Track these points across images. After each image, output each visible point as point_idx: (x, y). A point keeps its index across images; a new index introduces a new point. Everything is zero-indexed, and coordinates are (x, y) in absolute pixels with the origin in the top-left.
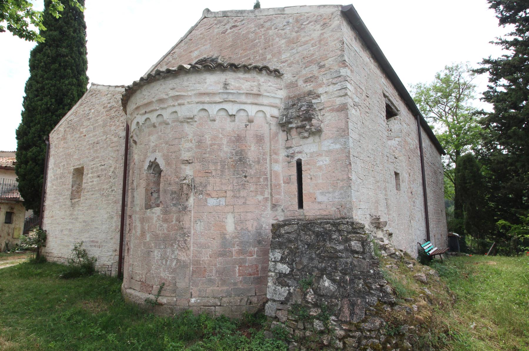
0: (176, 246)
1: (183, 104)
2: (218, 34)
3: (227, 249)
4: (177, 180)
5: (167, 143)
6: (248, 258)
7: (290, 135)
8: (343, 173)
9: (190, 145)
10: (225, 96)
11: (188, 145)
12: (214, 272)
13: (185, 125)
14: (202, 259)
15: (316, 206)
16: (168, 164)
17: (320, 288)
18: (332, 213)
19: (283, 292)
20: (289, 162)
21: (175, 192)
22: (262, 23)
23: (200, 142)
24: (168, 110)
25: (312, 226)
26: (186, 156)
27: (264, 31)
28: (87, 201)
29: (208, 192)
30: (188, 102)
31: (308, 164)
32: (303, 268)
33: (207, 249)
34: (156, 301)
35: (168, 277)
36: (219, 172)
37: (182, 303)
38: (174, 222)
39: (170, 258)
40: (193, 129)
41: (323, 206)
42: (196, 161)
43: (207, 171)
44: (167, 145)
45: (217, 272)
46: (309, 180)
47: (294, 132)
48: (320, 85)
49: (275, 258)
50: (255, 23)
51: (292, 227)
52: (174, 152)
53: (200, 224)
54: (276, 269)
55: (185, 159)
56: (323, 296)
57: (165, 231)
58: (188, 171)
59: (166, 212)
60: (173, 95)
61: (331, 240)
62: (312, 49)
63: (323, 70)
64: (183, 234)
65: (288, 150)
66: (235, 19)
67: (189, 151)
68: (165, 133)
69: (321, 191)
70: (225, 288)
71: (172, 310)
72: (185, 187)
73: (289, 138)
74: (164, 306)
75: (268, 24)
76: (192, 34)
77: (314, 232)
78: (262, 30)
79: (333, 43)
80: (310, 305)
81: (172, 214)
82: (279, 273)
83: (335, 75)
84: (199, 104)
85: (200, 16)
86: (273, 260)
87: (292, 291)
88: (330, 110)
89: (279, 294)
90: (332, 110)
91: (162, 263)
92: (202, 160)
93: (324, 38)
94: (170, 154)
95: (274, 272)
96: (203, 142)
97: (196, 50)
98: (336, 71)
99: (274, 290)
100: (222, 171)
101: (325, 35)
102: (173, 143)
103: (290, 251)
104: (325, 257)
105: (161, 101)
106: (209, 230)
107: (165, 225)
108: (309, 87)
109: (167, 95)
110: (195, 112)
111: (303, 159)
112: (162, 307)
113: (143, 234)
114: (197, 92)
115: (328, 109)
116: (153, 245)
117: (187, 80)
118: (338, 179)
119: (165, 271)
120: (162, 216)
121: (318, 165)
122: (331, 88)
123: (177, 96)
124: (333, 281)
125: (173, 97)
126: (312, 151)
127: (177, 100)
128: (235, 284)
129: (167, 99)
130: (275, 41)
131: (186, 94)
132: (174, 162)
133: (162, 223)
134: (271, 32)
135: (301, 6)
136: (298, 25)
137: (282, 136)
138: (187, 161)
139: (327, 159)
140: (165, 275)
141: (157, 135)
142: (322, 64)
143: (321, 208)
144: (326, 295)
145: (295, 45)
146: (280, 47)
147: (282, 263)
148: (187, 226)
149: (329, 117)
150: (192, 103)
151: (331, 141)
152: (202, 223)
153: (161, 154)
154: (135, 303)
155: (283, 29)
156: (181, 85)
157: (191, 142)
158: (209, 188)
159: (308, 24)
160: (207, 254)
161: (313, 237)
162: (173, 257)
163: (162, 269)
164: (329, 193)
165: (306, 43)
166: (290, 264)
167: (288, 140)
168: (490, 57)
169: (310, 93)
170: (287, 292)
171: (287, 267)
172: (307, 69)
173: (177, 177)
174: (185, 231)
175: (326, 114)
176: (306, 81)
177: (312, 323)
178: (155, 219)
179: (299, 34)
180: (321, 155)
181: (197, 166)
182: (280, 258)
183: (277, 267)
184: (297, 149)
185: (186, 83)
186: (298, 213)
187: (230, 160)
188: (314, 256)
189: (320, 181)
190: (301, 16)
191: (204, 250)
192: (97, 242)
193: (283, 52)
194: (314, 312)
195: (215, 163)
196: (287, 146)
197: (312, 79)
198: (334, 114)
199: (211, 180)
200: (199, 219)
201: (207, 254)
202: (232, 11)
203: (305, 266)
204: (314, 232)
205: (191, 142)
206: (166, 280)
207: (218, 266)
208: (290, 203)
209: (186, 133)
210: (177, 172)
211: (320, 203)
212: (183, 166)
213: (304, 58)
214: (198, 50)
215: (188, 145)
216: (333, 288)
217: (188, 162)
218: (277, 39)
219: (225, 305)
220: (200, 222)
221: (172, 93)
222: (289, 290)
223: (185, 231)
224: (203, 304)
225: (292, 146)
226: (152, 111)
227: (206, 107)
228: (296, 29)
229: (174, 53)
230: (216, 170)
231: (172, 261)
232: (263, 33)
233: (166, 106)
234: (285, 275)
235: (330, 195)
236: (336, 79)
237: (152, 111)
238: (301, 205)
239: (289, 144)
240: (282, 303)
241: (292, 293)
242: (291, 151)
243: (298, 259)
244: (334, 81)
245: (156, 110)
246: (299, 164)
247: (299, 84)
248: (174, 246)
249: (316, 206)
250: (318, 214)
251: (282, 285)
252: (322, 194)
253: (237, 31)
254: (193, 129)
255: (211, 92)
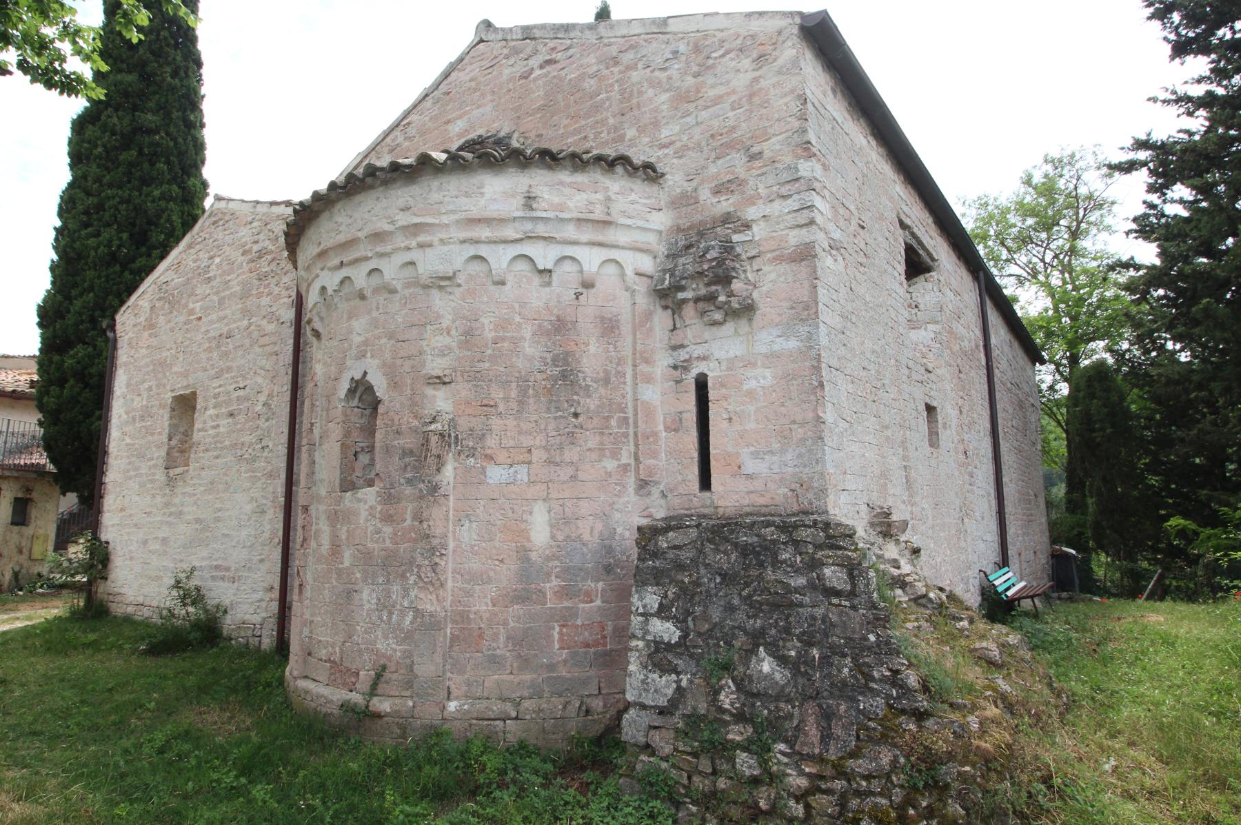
0: (412, 578)
1: (430, 245)
2: (510, 80)
3: (533, 586)
4: (416, 423)
5: (391, 336)
6: (581, 605)
7: (680, 316)
8: (805, 406)
9: (447, 340)
10: (529, 226)
11: (441, 341)
12: (502, 638)
13: (435, 293)
14: (473, 609)
15: (742, 485)
16: (394, 385)
17: (750, 677)
18: (779, 500)
19: (665, 685)
20: (677, 382)
21: (411, 452)
22: (615, 54)
23: (469, 333)
24: (393, 257)
25: (732, 532)
26: (436, 366)
27: (620, 72)
28: (203, 473)
29: (488, 452)
30: (441, 240)
31: (723, 385)
32: (711, 630)
33: (486, 586)
34: (367, 707)
35: (395, 651)
36: (514, 405)
37: (428, 713)
38: (408, 522)
39: (398, 607)
40: (454, 304)
41: (758, 485)
42: (460, 379)
43: (485, 402)
44: (393, 342)
45: (508, 638)
46: (725, 424)
47: (689, 311)
48: (752, 201)
49: (644, 606)
50: (598, 53)
51: (686, 534)
52: (409, 358)
53: (470, 527)
54: (646, 632)
55: (435, 373)
56: (757, 695)
57: (388, 543)
58: (442, 401)
59: (389, 498)
60: (405, 223)
61: (776, 563)
62: (731, 114)
63: (757, 164)
64: (428, 550)
65: (675, 354)
66: (551, 44)
67: (444, 355)
68: (387, 313)
69: (752, 449)
70: (528, 677)
71: (403, 728)
72: (434, 439)
73: (678, 326)
74: (385, 719)
75: (628, 58)
76: (449, 79)
77: (736, 545)
78: (616, 70)
79: (782, 102)
80: (727, 718)
81: (403, 503)
82: (655, 642)
83: (786, 176)
84: (467, 245)
85: (469, 37)
86: (641, 610)
87: (684, 683)
88: (775, 258)
89: (656, 691)
90: (780, 259)
91: (380, 618)
92: (474, 376)
93: (761, 89)
94: (399, 362)
95: (643, 638)
96: (477, 333)
97: (460, 117)
98: (789, 168)
99: (643, 682)
100: (521, 403)
101: (763, 83)
102: (406, 337)
103: (680, 589)
104: (761, 604)
105: (378, 236)
106: (491, 540)
107: (388, 530)
108: (725, 204)
109: (392, 223)
110: (458, 263)
111: (710, 374)
112: (380, 722)
113: (336, 549)
114: (463, 215)
115: (769, 255)
116: (358, 575)
117: (440, 189)
118: (794, 422)
119: (386, 638)
120: (379, 508)
121: (745, 387)
122: (777, 207)
123: (416, 225)
124: (782, 660)
125: (405, 228)
126: (731, 354)
127: (415, 235)
128: (551, 667)
129: (391, 233)
130: (645, 97)
131: (437, 221)
132: (409, 382)
133: (379, 525)
134: (635, 76)
135: (705, 15)
136: (700, 59)
137: (662, 319)
138: (438, 377)
139: (768, 373)
140: (388, 646)
141: (367, 317)
142: (755, 149)
143: (752, 488)
144: (766, 694)
145: (691, 107)
146: (656, 110)
147: (663, 618)
148: (438, 531)
149: (773, 276)
150: (449, 243)
151: (775, 332)
152: (474, 525)
153: (377, 361)
154: (316, 712)
155: (664, 69)
156: (425, 199)
157: (448, 333)
158: (491, 442)
159: (722, 56)
160: (485, 597)
161: (733, 557)
162: (406, 604)
163: (379, 633)
164: (772, 452)
165: (717, 100)
166: (680, 621)
167: (675, 328)
168: (1149, 135)
169: (727, 219)
170: (674, 685)
171: (673, 628)
172: (720, 162)
173: (416, 417)
174: (435, 542)
175: (766, 269)
176: (717, 192)
177: (732, 760)
178: (364, 514)
179: (700, 79)
180: (754, 365)
181: (463, 389)
182: (657, 606)
183: (651, 628)
184: (697, 351)
185: (435, 196)
186: (700, 501)
187: (539, 377)
188: (736, 602)
189: (751, 426)
190: (706, 37)
191: (477, 588)
192: (228, 569)
193: (664, 122)
194: (736, 734)
195: (505, 384)
196: (673, 342)
197: (733, 187)
198: (784, 267)
199: (496, 422)
200: (467, 516)
201: (485, 597)
202: (543, 27)
203: (716, 624)
204: (736, 545)
205: (448, 333)
206: (389, 659)
207: (512, 624)
208: (680, 478)
209: (437, 313)
210: (416, 404)
211: (750, 477)
212: (429, 391)
213: (712, 136)
214: (465, 118)
215: (441, 341)
216: (781, 676)
217: (441, 381)
218: (651, 92)
219: (528, 717)
220: (470, 521)
221: (403, 219)
222: (678, 682)
223: (435, 542)
224: (475, 715)
225: (686, 342)
226: (356, 261)
227: (483, 250)
228: (695, 69)
229: (409, 124)
230: (506, 399)
231: (402, 613)
232: (617, 77)
233: (388, 248)
234: (669, 647)
235: (775, 458)
236: (788, 187)
237: (356, 261)
238: (705, 482)
239: (678, 338)
240: (662, 712)
241: (685, 690)
242: (683, 355)
243: (698, 609)
244: (784, 190)
245: (367, 259)
246: (702, 386)
247: (702, 197)
248: (407, 579)
249: (742, 485)
250: (746, 502)
251: (662, 671)
252: (756, 455)
253: (555, 74)
254: (454, 304)
255: (495, 215)
